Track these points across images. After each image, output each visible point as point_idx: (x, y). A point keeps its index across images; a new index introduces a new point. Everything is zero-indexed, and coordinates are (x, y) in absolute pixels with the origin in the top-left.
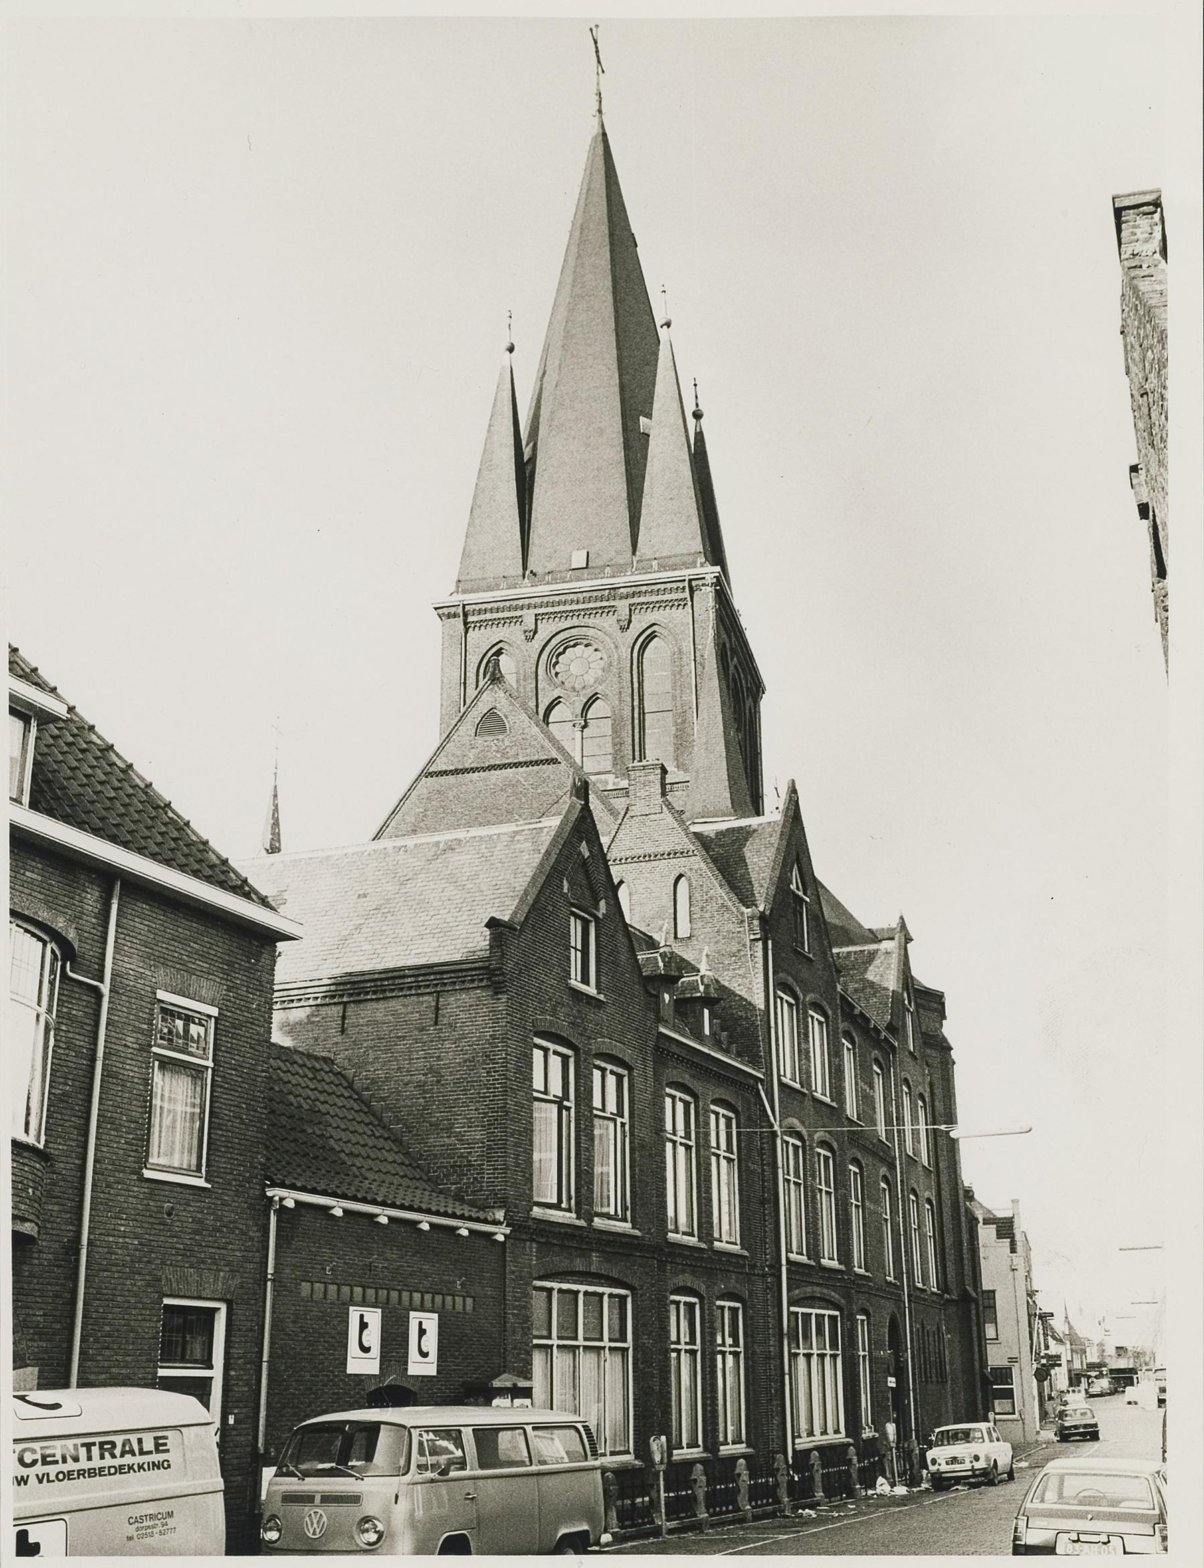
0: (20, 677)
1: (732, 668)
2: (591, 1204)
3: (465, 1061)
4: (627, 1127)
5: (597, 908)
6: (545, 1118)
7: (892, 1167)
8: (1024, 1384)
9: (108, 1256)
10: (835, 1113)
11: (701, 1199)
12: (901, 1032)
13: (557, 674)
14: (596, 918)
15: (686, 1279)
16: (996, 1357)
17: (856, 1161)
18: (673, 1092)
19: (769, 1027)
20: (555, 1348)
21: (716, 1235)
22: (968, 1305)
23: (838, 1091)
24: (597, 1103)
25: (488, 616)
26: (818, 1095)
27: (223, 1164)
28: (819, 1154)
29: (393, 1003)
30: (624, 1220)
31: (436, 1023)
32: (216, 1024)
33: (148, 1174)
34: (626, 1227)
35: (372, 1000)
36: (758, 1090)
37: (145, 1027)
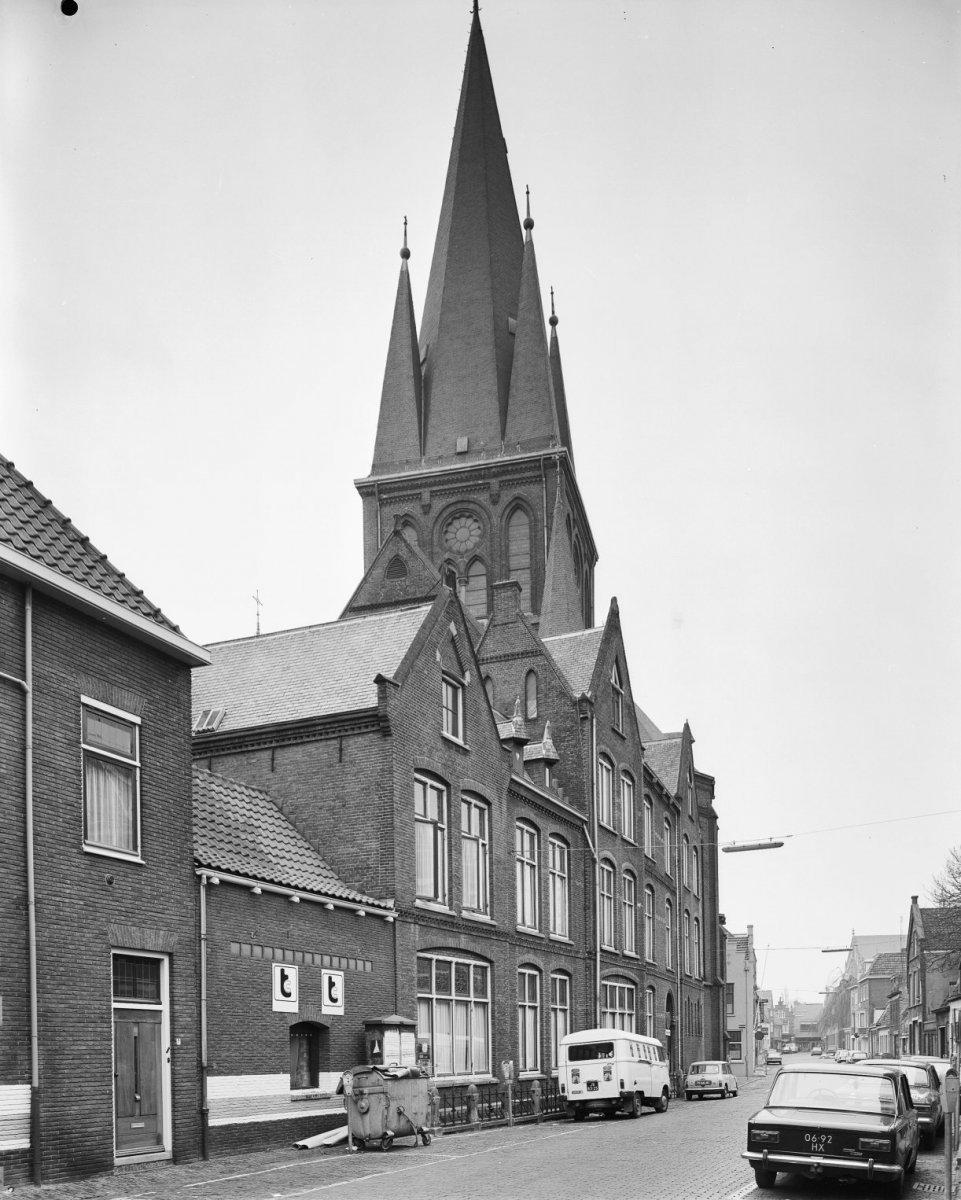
0: (148, 615)
1: (573, 534)
2: (460, 901)
3: (363, 789)
4: (487, 847)
5: (463, 675)
6: (425, 834)
7: (673, 893)
8: (748, 1041)
9: (57, 912)
10: (635, 849)
11: (542, 903)
12: (684, 801)
13: (446, 532)
14: (463, 685)
15: (530, 958)
16: (732, 1025)
17: (650, 886)
18: (521, 825)
19: (593, 784)
20: (434, 1001)
21: (551, 929)
22: (718, 990)
23: (639, 836)
24: (464, 827)
25: (396, 494)
26: (626, 837)
27: (156, 846)
28: (625, 879)
29: (311, 748)
30: (486, 914)
31: (340, 761)
32: (140, 731)
33: (87, 849)
34: (486, 919)
35: (293, 745)
36: (583, 829)
37: (73, 725)
